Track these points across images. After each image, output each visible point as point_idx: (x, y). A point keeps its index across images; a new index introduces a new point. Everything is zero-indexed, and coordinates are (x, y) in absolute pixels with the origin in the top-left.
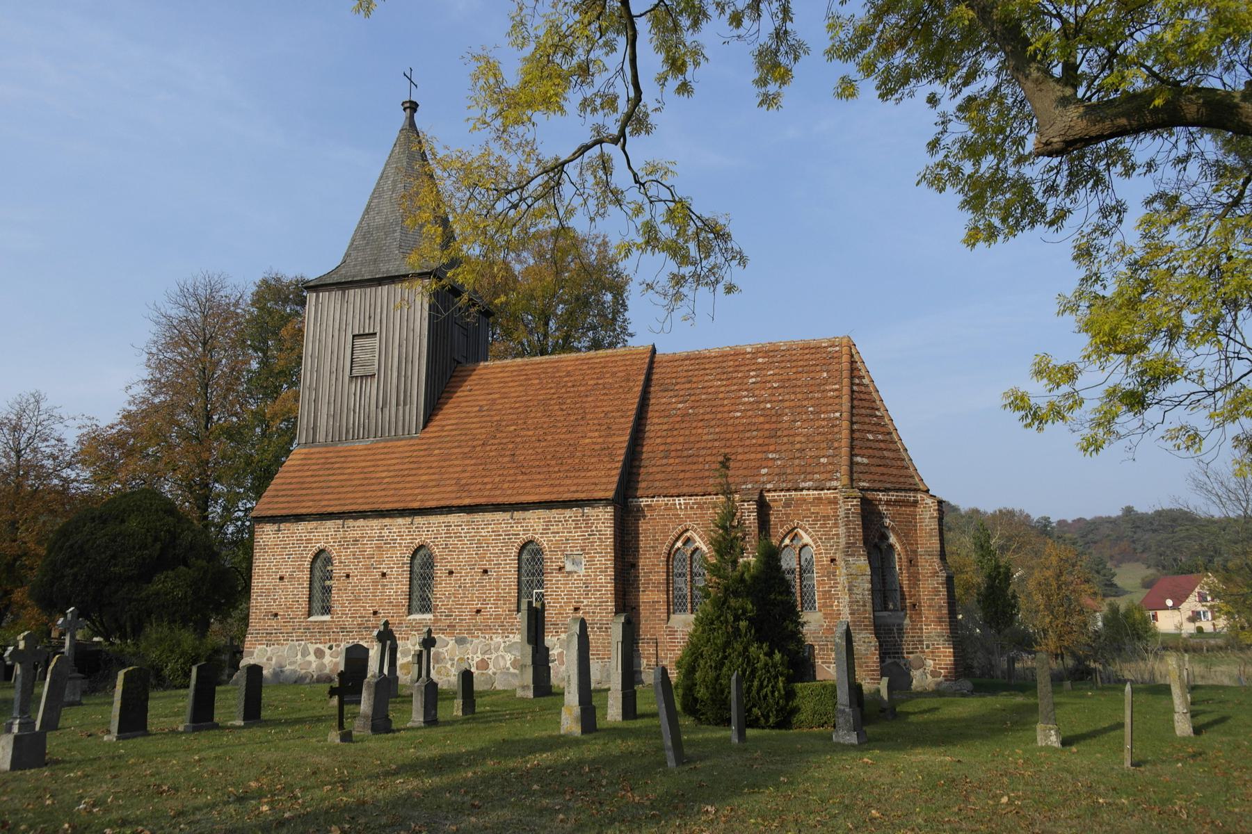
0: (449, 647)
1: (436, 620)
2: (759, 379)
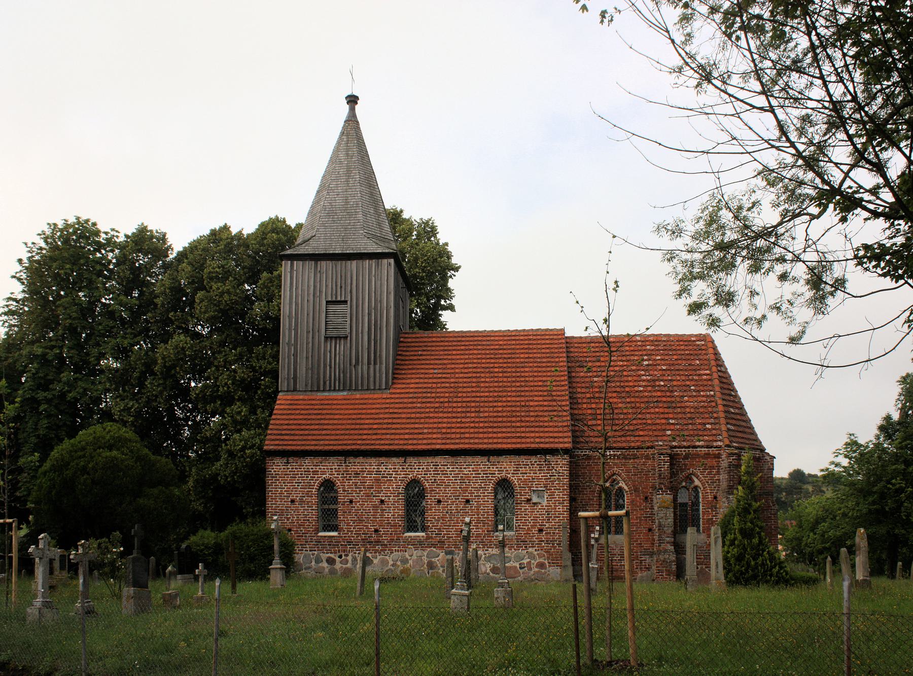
0: (440, 557)
1: (428, 538)
2: (651, 362)
